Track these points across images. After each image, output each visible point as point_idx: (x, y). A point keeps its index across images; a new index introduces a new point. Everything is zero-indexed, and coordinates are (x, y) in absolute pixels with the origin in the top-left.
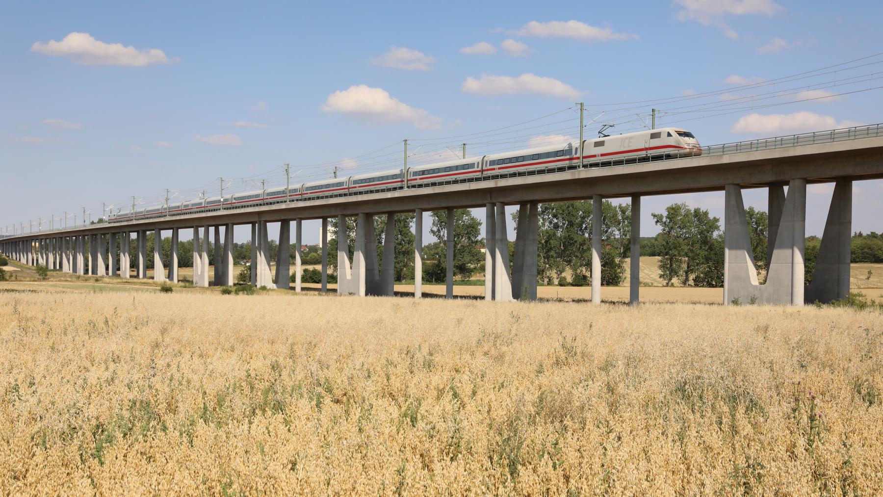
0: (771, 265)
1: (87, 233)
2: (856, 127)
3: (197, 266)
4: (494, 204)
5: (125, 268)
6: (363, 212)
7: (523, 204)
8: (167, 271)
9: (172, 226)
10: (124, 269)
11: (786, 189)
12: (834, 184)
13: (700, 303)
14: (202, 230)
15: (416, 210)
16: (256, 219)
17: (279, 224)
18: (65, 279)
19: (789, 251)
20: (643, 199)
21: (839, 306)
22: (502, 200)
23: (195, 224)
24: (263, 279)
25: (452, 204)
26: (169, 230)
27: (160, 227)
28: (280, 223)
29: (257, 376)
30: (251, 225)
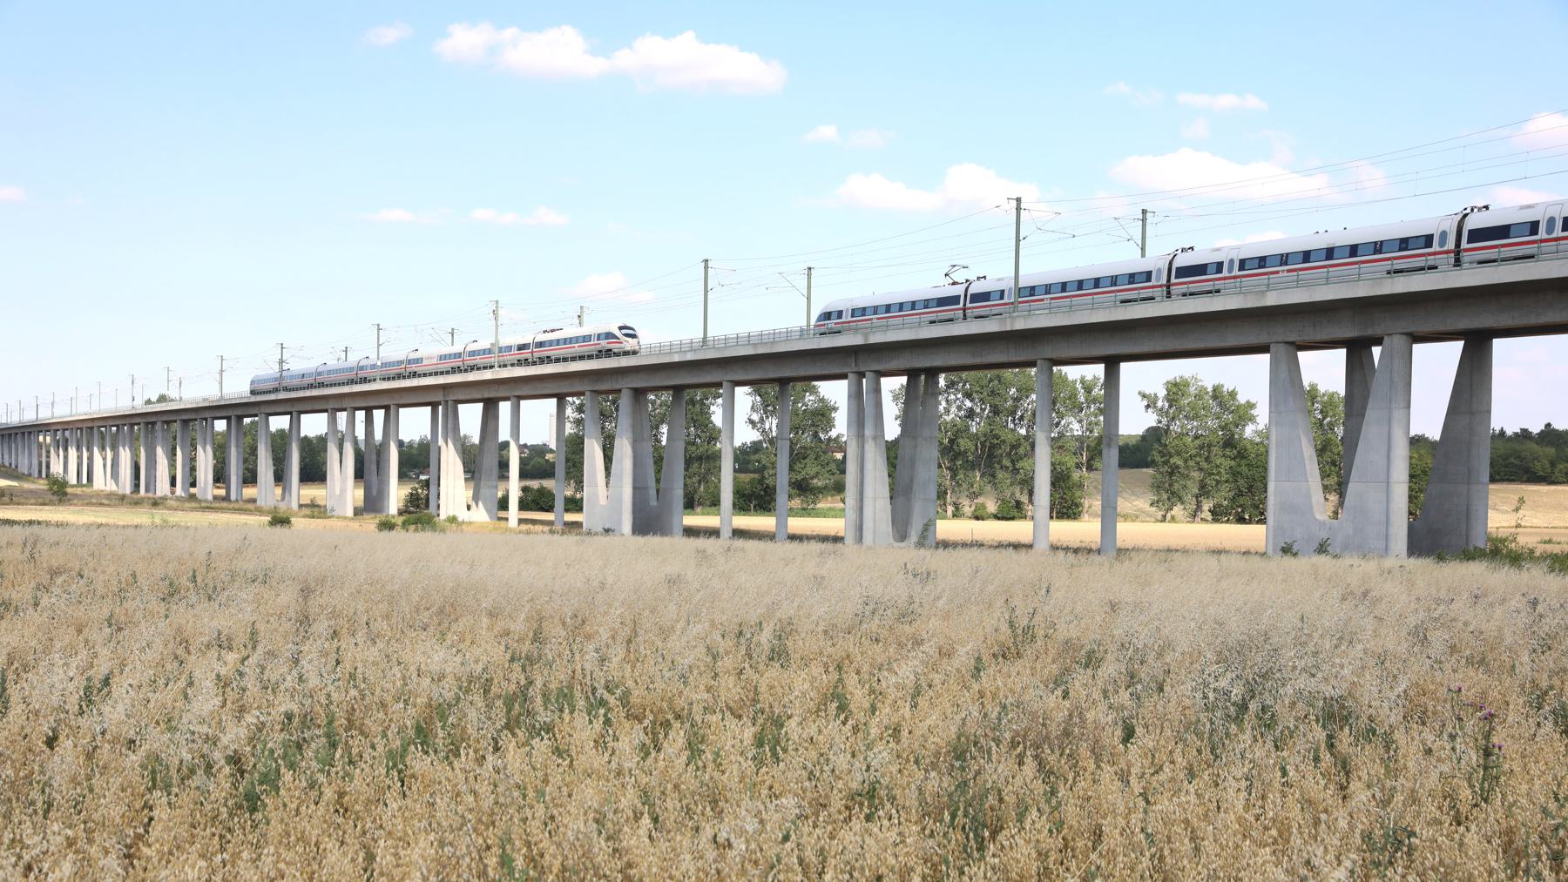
4: (862, 375)
7: (913, 374)
9: (289, 410)
11: (1376, 351)
12: (1461, 344)
28: (1344, 351)
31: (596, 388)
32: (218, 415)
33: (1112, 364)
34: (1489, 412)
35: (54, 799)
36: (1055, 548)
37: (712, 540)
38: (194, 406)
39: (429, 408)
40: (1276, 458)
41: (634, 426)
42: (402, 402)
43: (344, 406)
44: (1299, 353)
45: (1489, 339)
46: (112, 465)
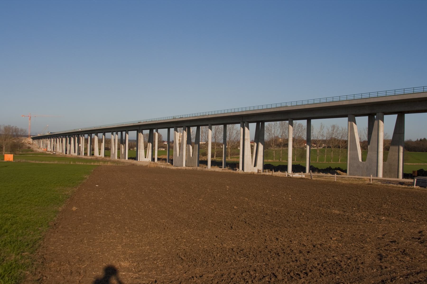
0: (368, 152)
1: (67, 134)
2: (395, 90)
3: (112, 150)
4: (244, 122)
5: (82, 151)
6: (185, 125)
7: (258, 123)
8: (153, 157)
9: (125, 130)
10: (82, 151)
11: (375, 116)
12: (196, 127)
13: (107, 156)
14: (193, 130)
15: (209, 125)
16: (138, 128)
17: (367, 118)
18: (426, 191)
19: (397, 147)
20: (407, 116)
21: (39, 151)
22: (157, 127)
23: (121, 130)
24: (140, 156)
25: (169, 127)
26: (194, 127)
27: (97, 132)
28: (149, 130)
29: (283, 250)
30: (167, 129)
31: (177, 126)
32: (252, 120)
33: (309, 120)
34: (404, 133)
35: (322, 212)
36: (192, 156)
37: (98, 154)
38: (132, 125)
39: (167, 129)
40: (350, 145)
41: (123, 141)
42: (129, 130)
43: (182, 125)
44: (356, 118)
45: (153, 130)
46: (180, 147)
